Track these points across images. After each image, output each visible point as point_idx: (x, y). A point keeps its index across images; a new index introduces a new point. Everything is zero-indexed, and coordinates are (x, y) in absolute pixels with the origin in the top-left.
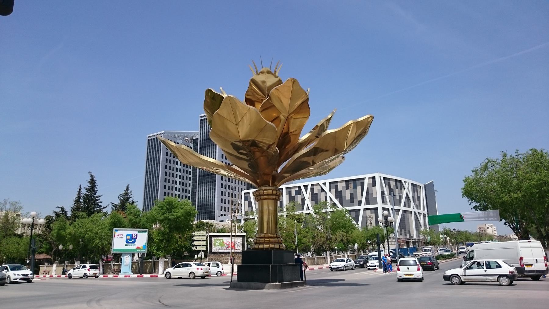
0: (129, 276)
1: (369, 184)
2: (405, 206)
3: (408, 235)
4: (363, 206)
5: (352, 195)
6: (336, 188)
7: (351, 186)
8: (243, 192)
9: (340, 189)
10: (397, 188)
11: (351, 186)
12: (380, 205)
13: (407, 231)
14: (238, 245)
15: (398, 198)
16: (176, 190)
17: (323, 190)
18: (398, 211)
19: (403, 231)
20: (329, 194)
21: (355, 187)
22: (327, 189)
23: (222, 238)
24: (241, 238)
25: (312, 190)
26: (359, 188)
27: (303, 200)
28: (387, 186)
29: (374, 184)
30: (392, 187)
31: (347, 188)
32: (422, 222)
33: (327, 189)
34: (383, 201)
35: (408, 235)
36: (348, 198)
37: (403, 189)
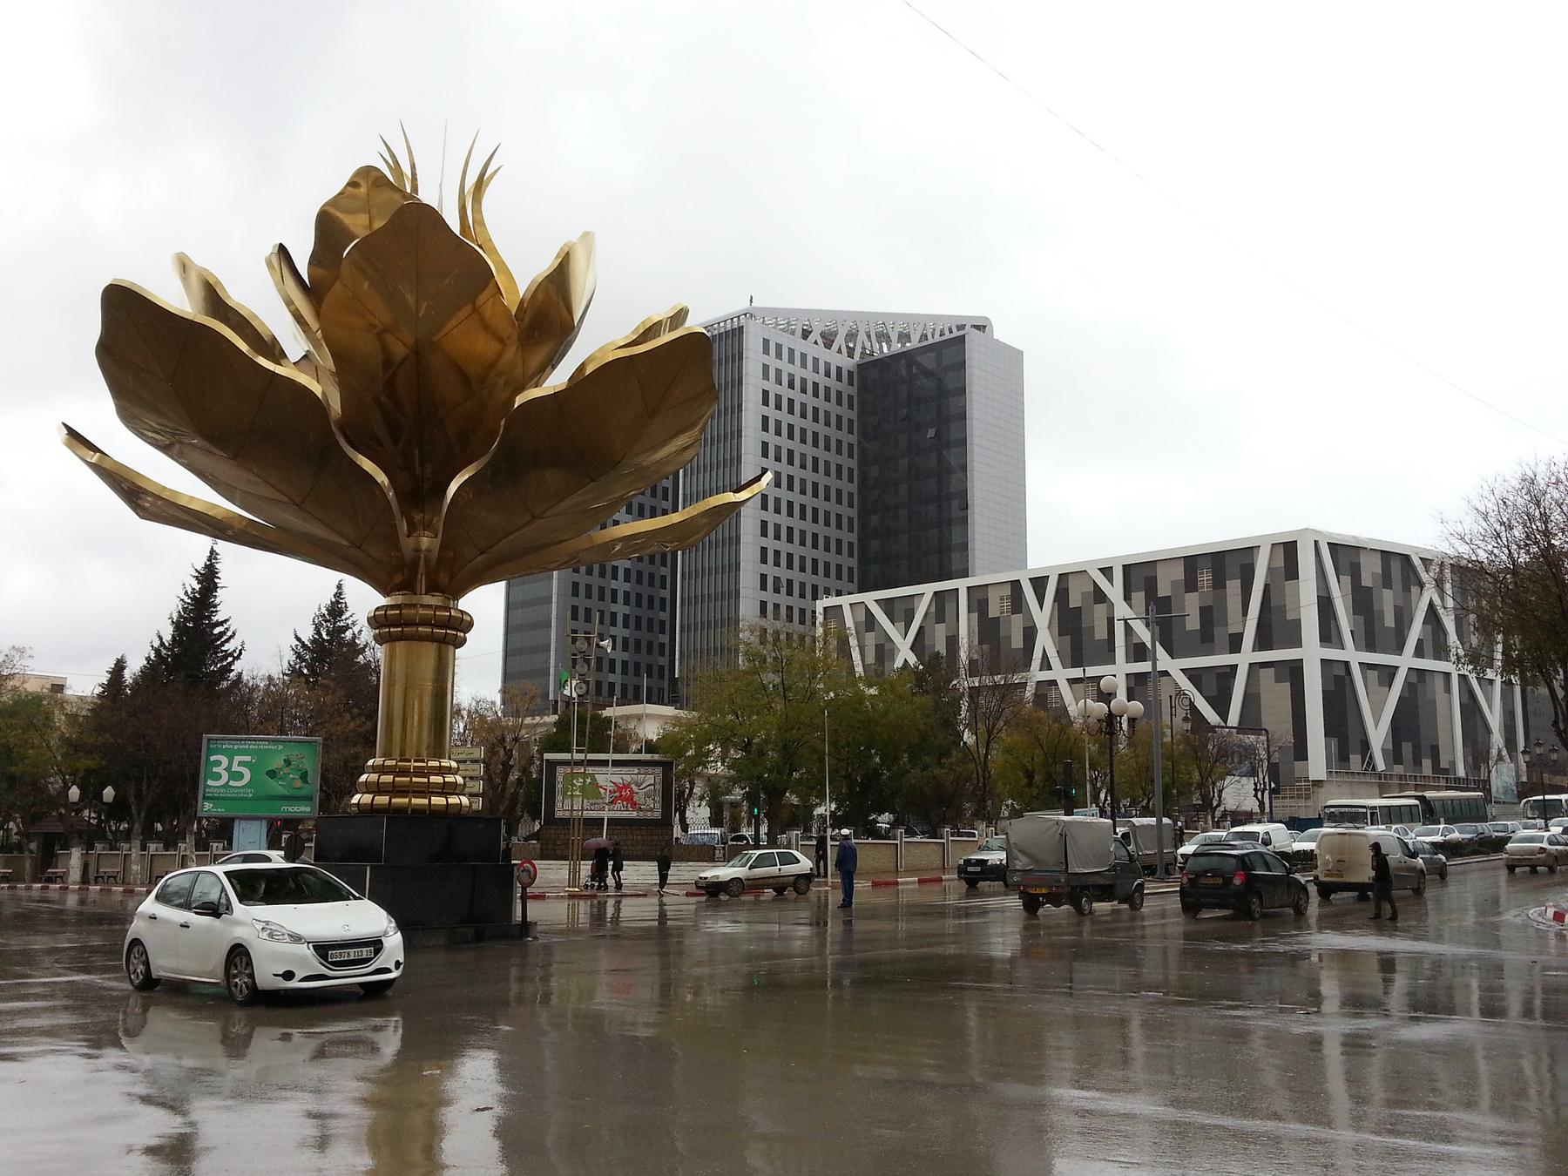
0: (876, 885)
1: (1271, 570)
2: (1419, 653)
3: (1427, 764)
4: (1245, 658)
5: (1206, 614)
6: (1150, 586)
7: (1205, 578)
8: (820, 605)
9: (1163, 590)
10: (1387, 583)
11: (1205, 578)
12: (1311, 653)
13: (1425, 749)
14: (647, 795)
15: (1390, 621)
16: (614, 600)
17: (1099, 596)
18: (1388, 673)
19: (1407, 749)
20: (1121, 610)
21: (1219, 583)
22: (1115, 591)
23: (590, 770)
24: (659, 770)
25: (1062, 594)
26: (1233, 587)
27: (1030, 633)
28: (1346, 580)
29: (1291, 571)
30: (1366, 581)
31: (1191, 584)
32: (1495, 719)
33: (1115, 591)
34: (1329, 634)
35: (1427, 764)
36: (1193, 623)
37: (1415, 590)
